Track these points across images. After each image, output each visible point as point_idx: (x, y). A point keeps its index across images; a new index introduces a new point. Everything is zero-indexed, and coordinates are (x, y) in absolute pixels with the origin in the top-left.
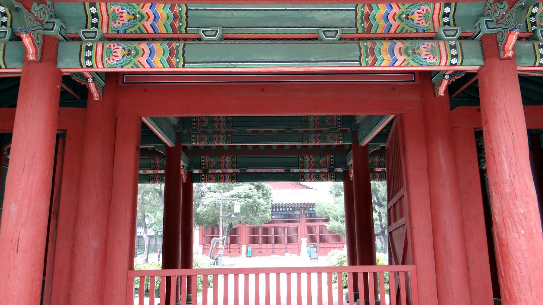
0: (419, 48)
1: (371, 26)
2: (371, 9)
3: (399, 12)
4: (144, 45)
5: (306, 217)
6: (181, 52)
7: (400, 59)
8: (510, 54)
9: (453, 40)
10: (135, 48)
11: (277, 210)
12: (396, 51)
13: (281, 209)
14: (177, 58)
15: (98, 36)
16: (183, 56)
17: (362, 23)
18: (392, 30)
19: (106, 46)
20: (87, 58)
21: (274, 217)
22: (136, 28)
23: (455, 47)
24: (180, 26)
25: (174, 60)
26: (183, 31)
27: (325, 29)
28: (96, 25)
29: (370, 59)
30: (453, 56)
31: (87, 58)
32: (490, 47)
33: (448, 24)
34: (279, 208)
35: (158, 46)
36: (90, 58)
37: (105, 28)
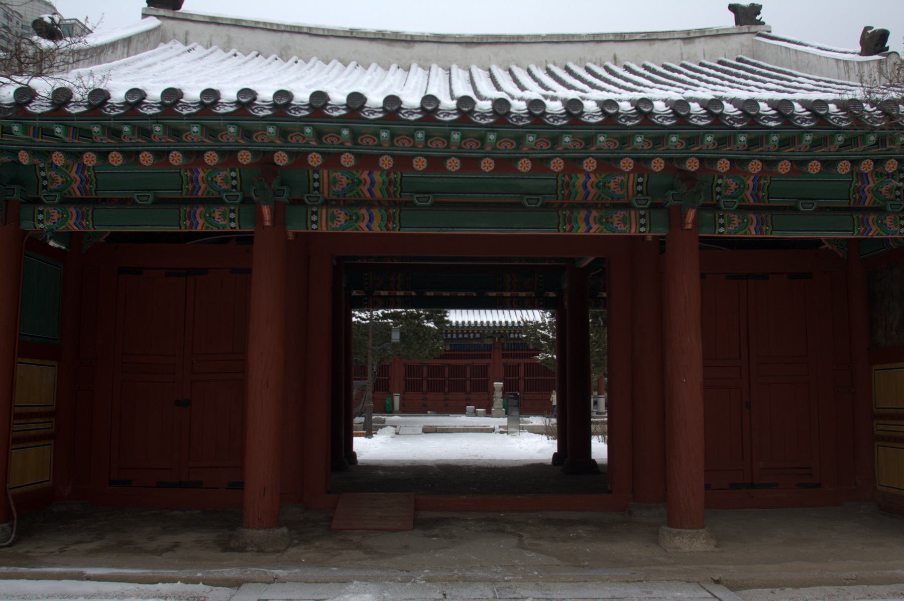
0: (612, 217)
1: (570, 193)
2: (571, 178)
3: (596, 181)
4: (363, 211)
5: (503, 349)
6: (397, 218)
7: (595, 227)
8: (689, 226)
9: (643, 209)
10: (356, 214)
11: (455, 336)
12: (591, 220)
13: (461, 336)
14: (394, 223)
15: (320, 201)
16: (399, 221)
17: (563, 189)
18: (590, 197)
19: (330, 211)
20: (313, 222)
21: (448, 348)
22: (355, 192)
23: (644, 216)
24: (395, 192)
25: (391, 225)
26: (398, 195)
27: (528, 197)
28: (317, 189)
29: (568, 227)
30: (641, 226)
31: (313, 222)
32: (675, 217)
33: (641, 192)
34: (457, 334)
35: (376, 212)
36: (316, 222)
37: (326, 192)
